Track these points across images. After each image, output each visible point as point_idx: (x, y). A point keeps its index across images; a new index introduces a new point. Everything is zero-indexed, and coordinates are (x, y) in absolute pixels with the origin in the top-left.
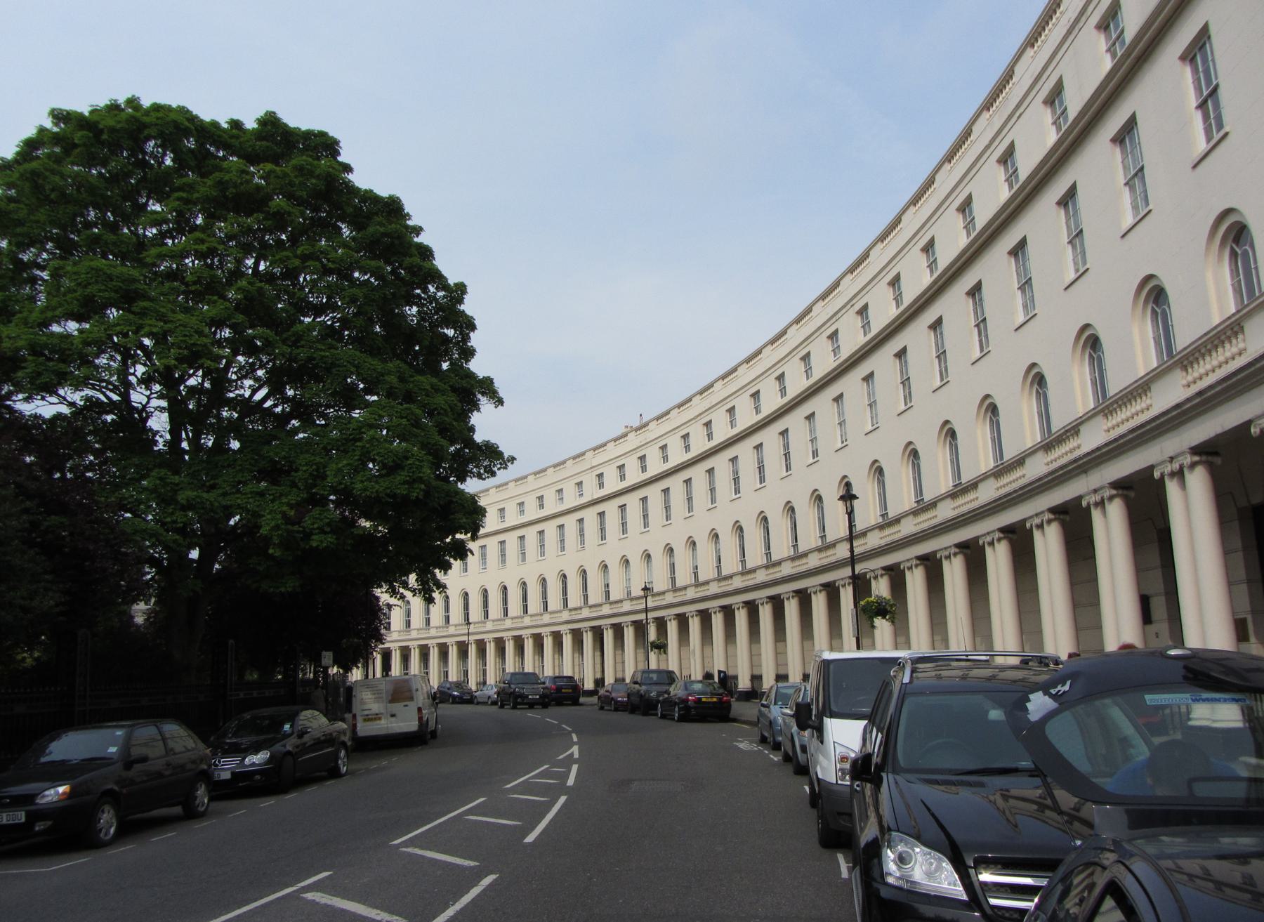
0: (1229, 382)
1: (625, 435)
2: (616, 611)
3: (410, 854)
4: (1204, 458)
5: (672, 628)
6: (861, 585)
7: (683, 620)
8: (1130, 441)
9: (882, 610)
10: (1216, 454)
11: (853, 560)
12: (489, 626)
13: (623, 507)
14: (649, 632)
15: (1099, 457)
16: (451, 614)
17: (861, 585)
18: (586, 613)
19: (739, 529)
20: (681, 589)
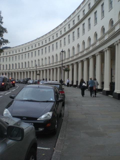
0: (112, 36)
1: (36, 39)
2: (27, 69)
3: (48, 148)
4: (100, 53)
5: (41, 72)
6: (36, 71)
7: (43, 71)
8: (98, 47)
9: (38, 75)
10: (102, 53)
11: (62, 64)
12: (10, 70)
13: (32, 53)
14: (10, 74)
15: (97, 47)
16: (14, 67)
17: (36, 71)
18: (22, 70)
19: (39, 60)
20: (30, 68)
